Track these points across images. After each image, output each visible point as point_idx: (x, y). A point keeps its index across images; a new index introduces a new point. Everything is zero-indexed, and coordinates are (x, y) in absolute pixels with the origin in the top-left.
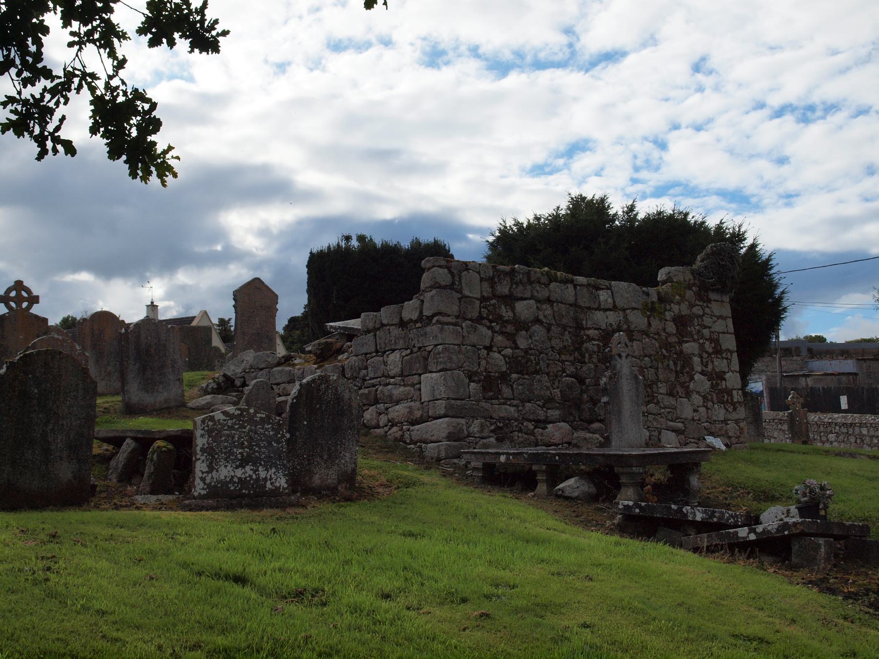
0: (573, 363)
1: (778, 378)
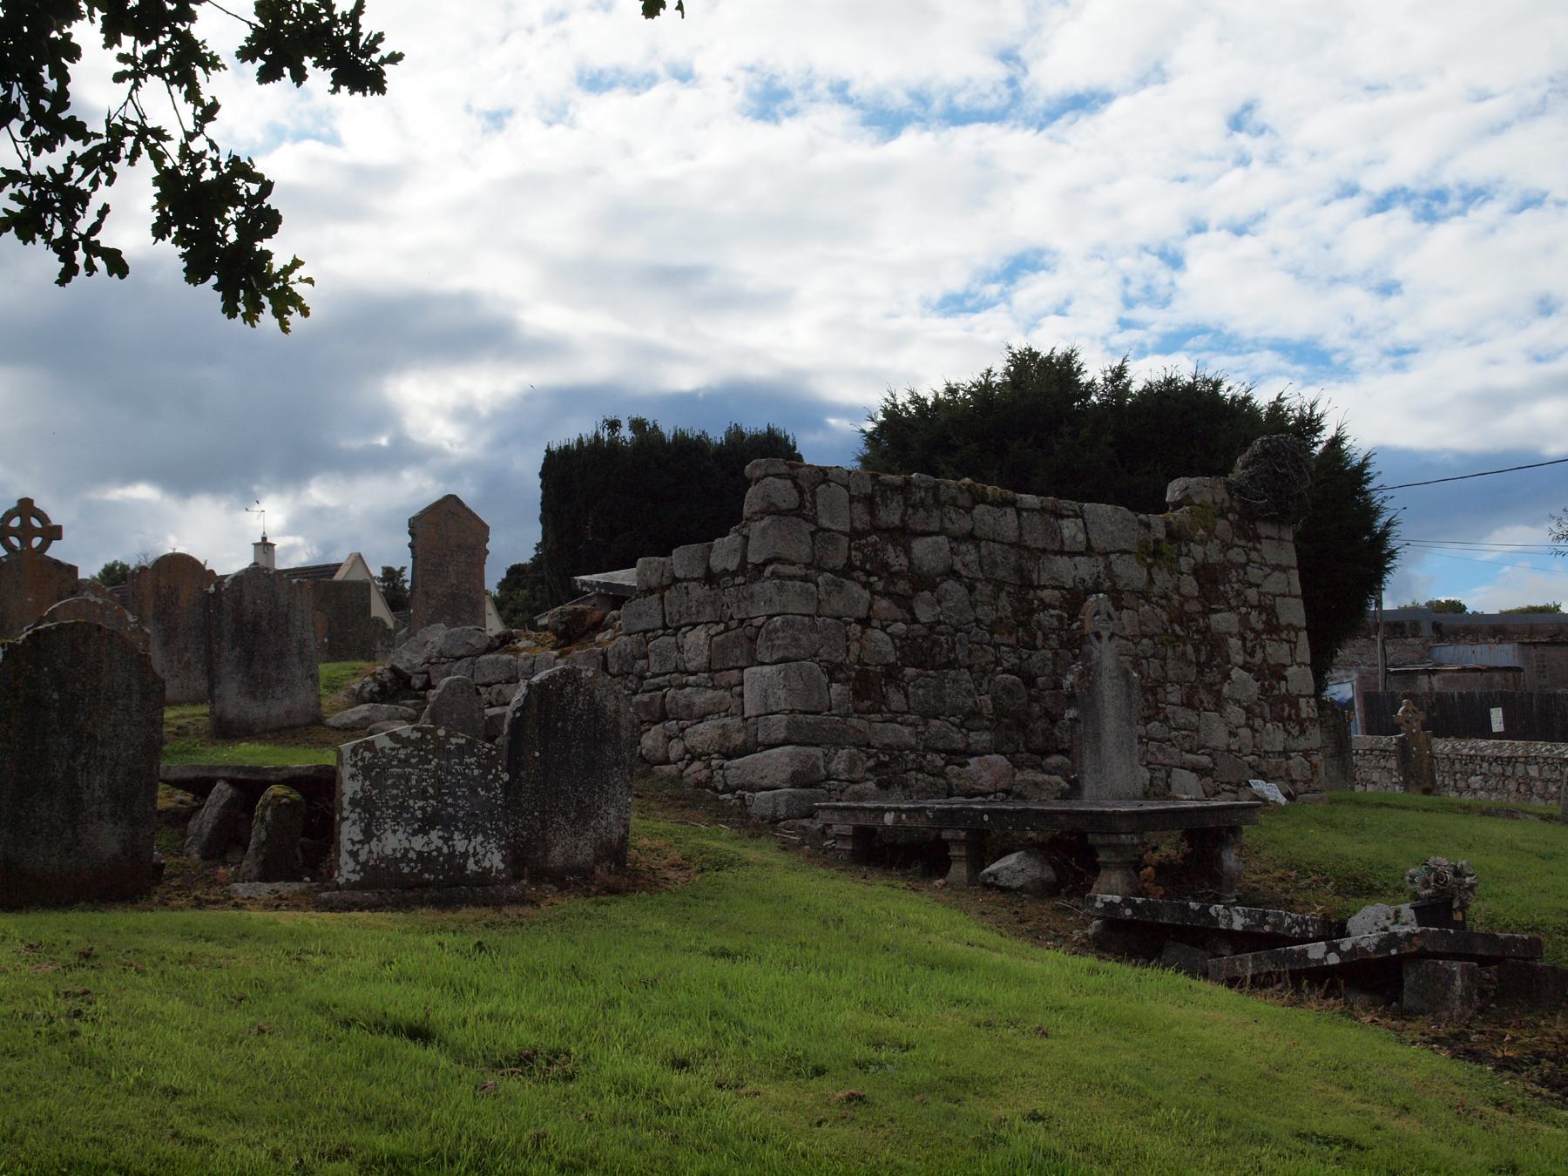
1: (1379, 676)
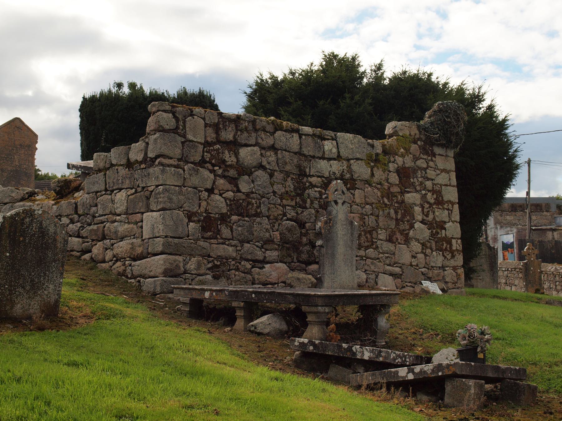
0: (294, 207)
1: (527, 231)
